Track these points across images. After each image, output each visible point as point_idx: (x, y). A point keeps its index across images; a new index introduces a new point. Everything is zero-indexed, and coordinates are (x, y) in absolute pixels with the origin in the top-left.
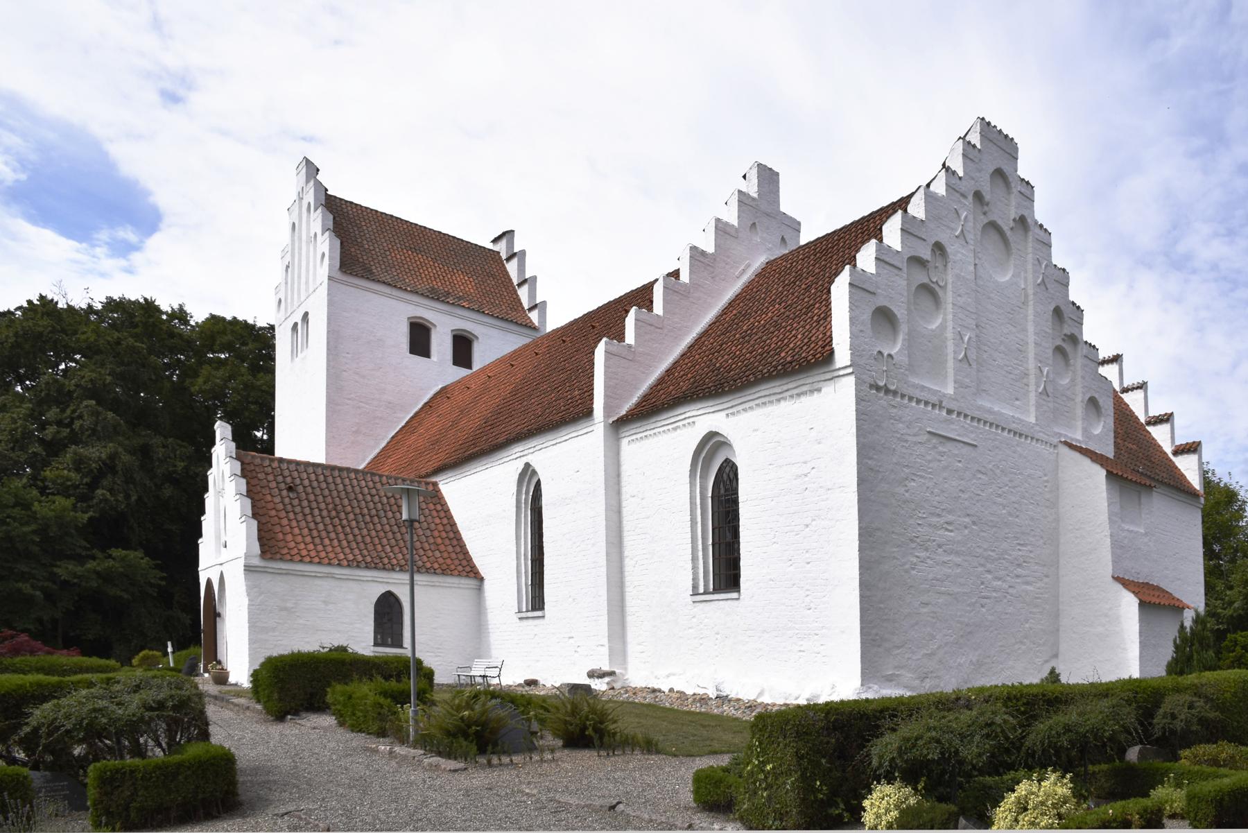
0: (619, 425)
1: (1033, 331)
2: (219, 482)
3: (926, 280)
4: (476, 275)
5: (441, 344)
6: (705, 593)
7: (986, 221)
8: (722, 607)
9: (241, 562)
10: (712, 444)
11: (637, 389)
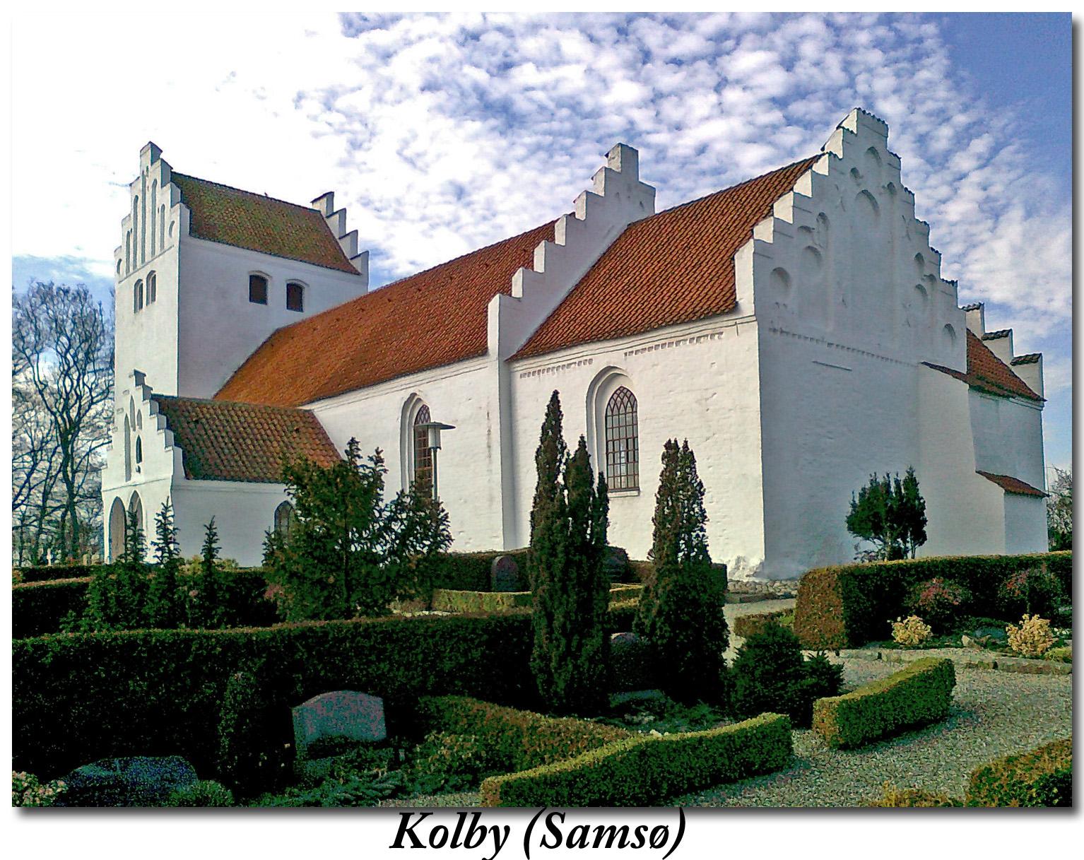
0: (509, 361)
1: (906, 275)
3: (810, 243)
4: (311, 233)
5: (276, 293)
7: (859, 190)
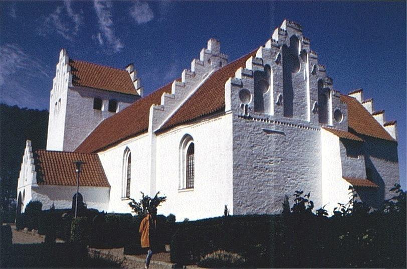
2: (26, 160)
6: (183, 189)
8: (188, 194)
9: (31, 186)
10: (188, 137)
11: (164, 119)
